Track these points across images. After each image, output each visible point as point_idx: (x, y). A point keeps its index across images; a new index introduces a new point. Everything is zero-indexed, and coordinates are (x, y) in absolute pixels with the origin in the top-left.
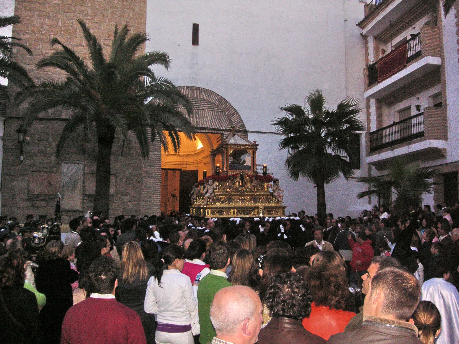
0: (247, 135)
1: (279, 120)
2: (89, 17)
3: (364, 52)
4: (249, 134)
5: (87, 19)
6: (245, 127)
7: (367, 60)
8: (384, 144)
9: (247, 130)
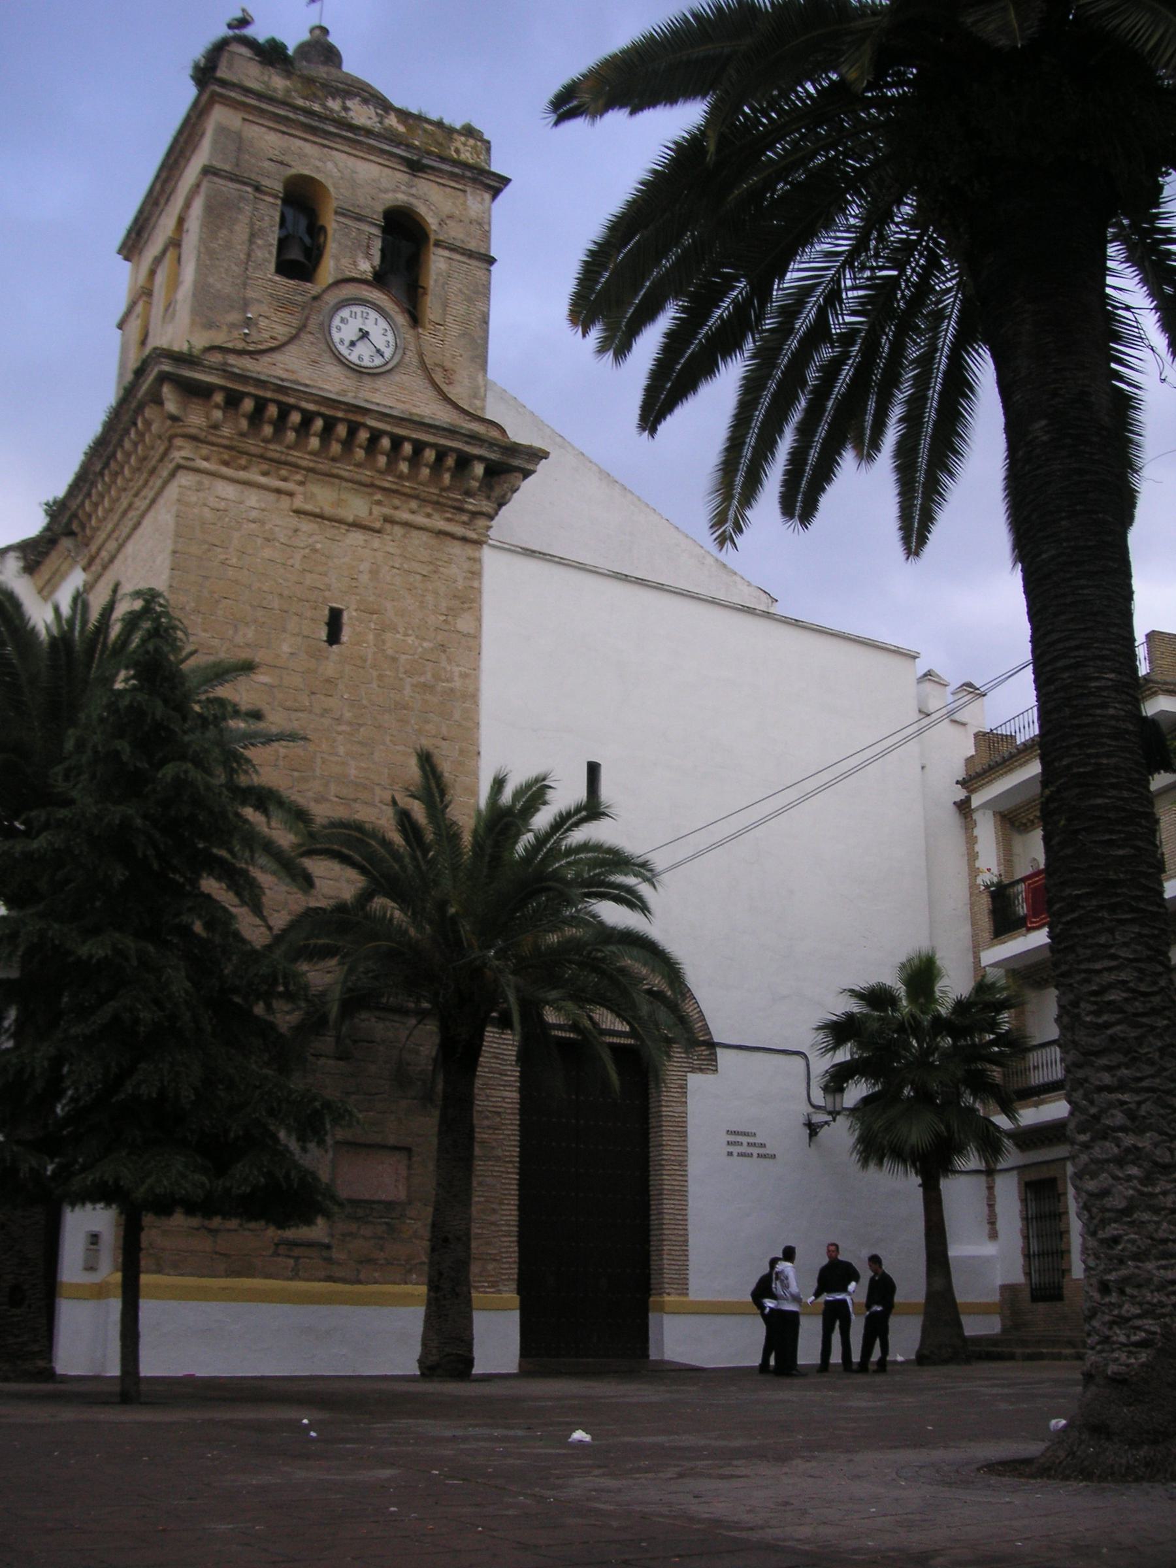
0: (715, 1054)
1: (835, 1018)
2: (343, 728)
3: (962, 848)
4: (719, 1051)
5: (339, 733)
6: (710, 1033)
7: (974, 872)
8: (1034, 1088)
9: (716, 1040)
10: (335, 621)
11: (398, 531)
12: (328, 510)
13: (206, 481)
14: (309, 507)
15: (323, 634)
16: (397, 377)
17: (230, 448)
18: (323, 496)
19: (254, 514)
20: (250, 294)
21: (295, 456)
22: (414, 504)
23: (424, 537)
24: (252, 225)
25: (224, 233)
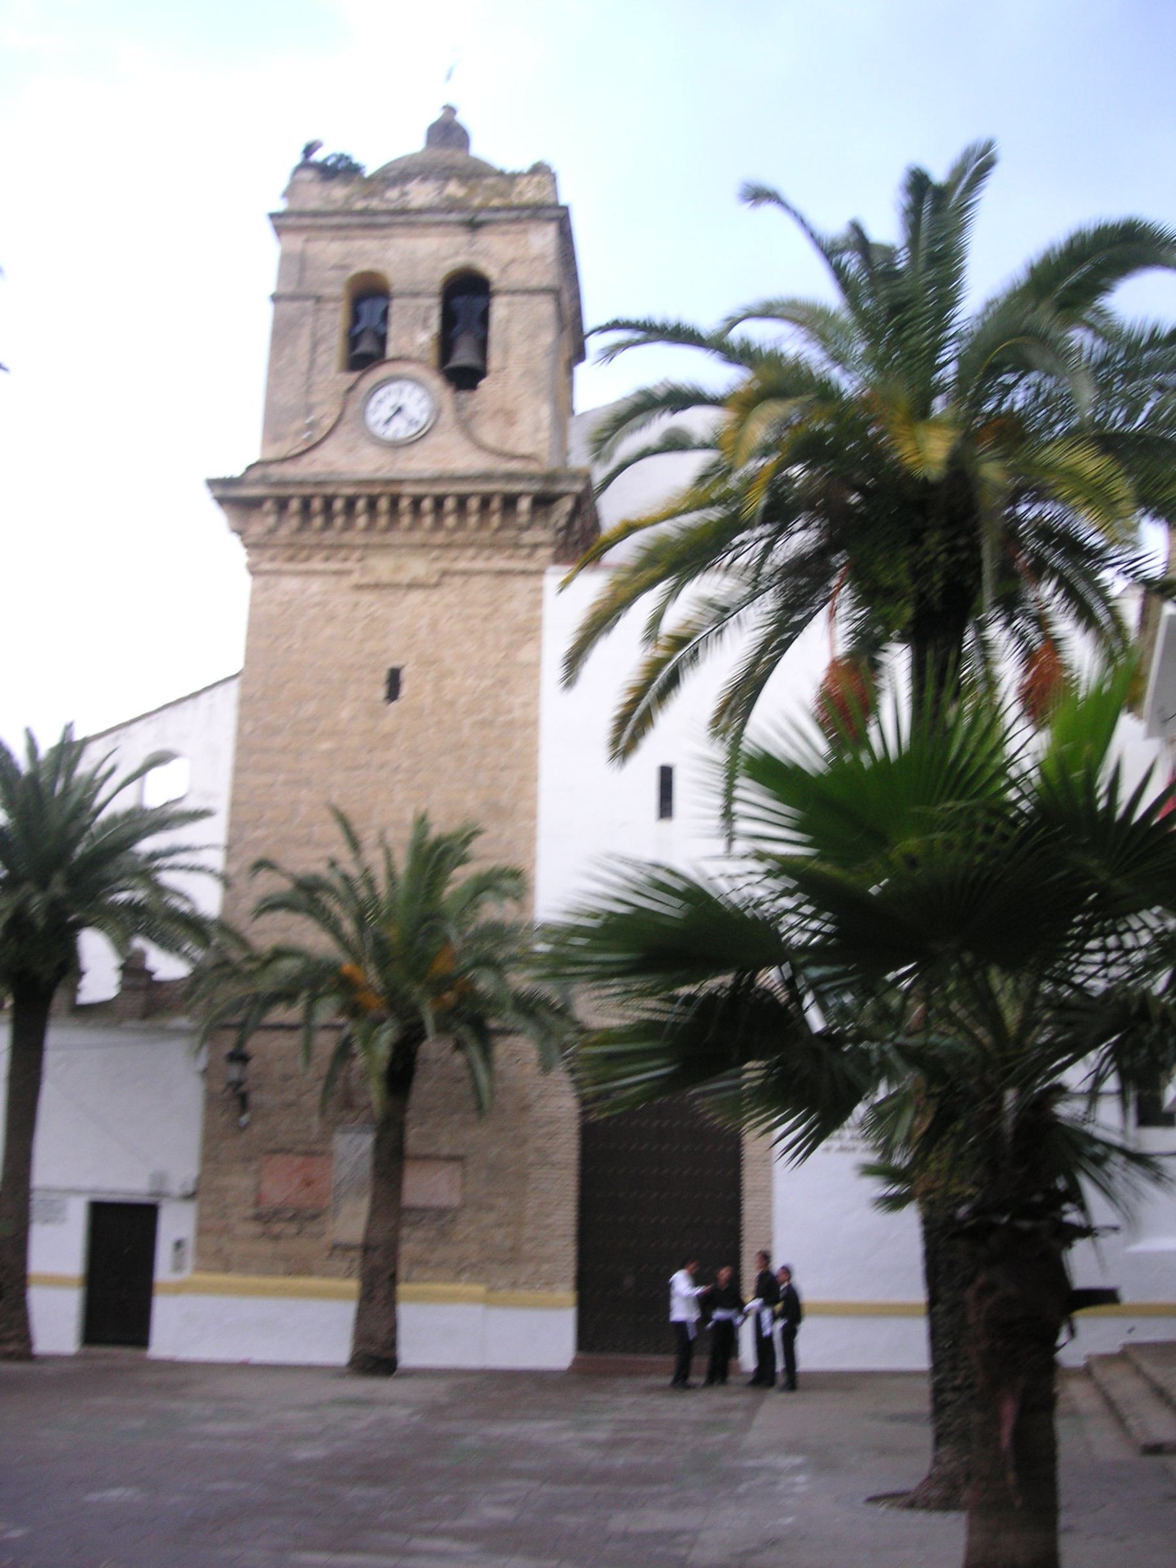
10: (394, 681)
11: (458, 581)
12: (386, 578)
13: (273, 580)
14: (365, 580)
15: (382, 692)
16: (432, 440)
17: (290, 545)
18: (382, 567)
19: (317, 599)
20: (315, 399)
21: (348, 537)
22: (471, 552)
23: (484, 581)
24: (313, 334)
25: (287, 351)
